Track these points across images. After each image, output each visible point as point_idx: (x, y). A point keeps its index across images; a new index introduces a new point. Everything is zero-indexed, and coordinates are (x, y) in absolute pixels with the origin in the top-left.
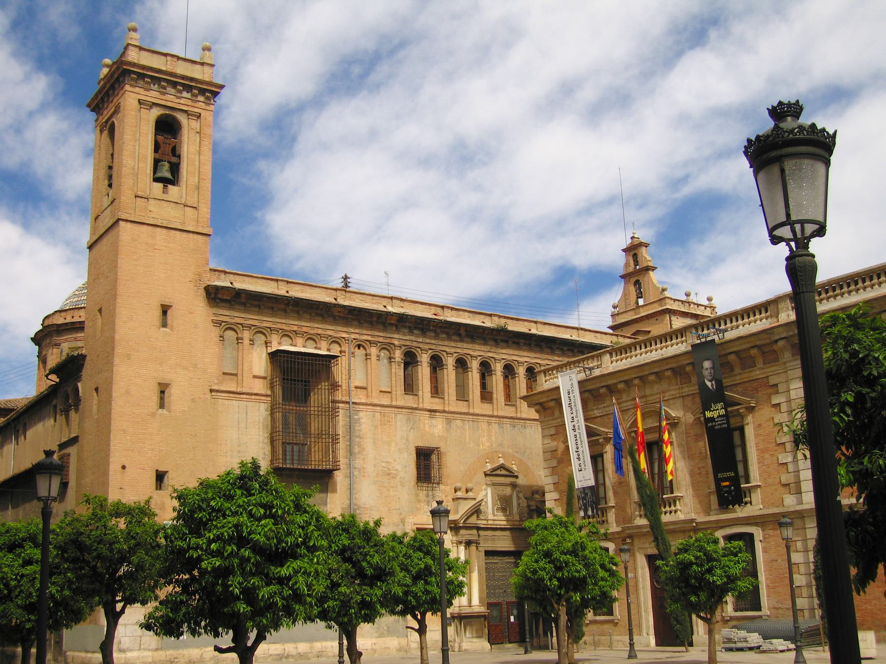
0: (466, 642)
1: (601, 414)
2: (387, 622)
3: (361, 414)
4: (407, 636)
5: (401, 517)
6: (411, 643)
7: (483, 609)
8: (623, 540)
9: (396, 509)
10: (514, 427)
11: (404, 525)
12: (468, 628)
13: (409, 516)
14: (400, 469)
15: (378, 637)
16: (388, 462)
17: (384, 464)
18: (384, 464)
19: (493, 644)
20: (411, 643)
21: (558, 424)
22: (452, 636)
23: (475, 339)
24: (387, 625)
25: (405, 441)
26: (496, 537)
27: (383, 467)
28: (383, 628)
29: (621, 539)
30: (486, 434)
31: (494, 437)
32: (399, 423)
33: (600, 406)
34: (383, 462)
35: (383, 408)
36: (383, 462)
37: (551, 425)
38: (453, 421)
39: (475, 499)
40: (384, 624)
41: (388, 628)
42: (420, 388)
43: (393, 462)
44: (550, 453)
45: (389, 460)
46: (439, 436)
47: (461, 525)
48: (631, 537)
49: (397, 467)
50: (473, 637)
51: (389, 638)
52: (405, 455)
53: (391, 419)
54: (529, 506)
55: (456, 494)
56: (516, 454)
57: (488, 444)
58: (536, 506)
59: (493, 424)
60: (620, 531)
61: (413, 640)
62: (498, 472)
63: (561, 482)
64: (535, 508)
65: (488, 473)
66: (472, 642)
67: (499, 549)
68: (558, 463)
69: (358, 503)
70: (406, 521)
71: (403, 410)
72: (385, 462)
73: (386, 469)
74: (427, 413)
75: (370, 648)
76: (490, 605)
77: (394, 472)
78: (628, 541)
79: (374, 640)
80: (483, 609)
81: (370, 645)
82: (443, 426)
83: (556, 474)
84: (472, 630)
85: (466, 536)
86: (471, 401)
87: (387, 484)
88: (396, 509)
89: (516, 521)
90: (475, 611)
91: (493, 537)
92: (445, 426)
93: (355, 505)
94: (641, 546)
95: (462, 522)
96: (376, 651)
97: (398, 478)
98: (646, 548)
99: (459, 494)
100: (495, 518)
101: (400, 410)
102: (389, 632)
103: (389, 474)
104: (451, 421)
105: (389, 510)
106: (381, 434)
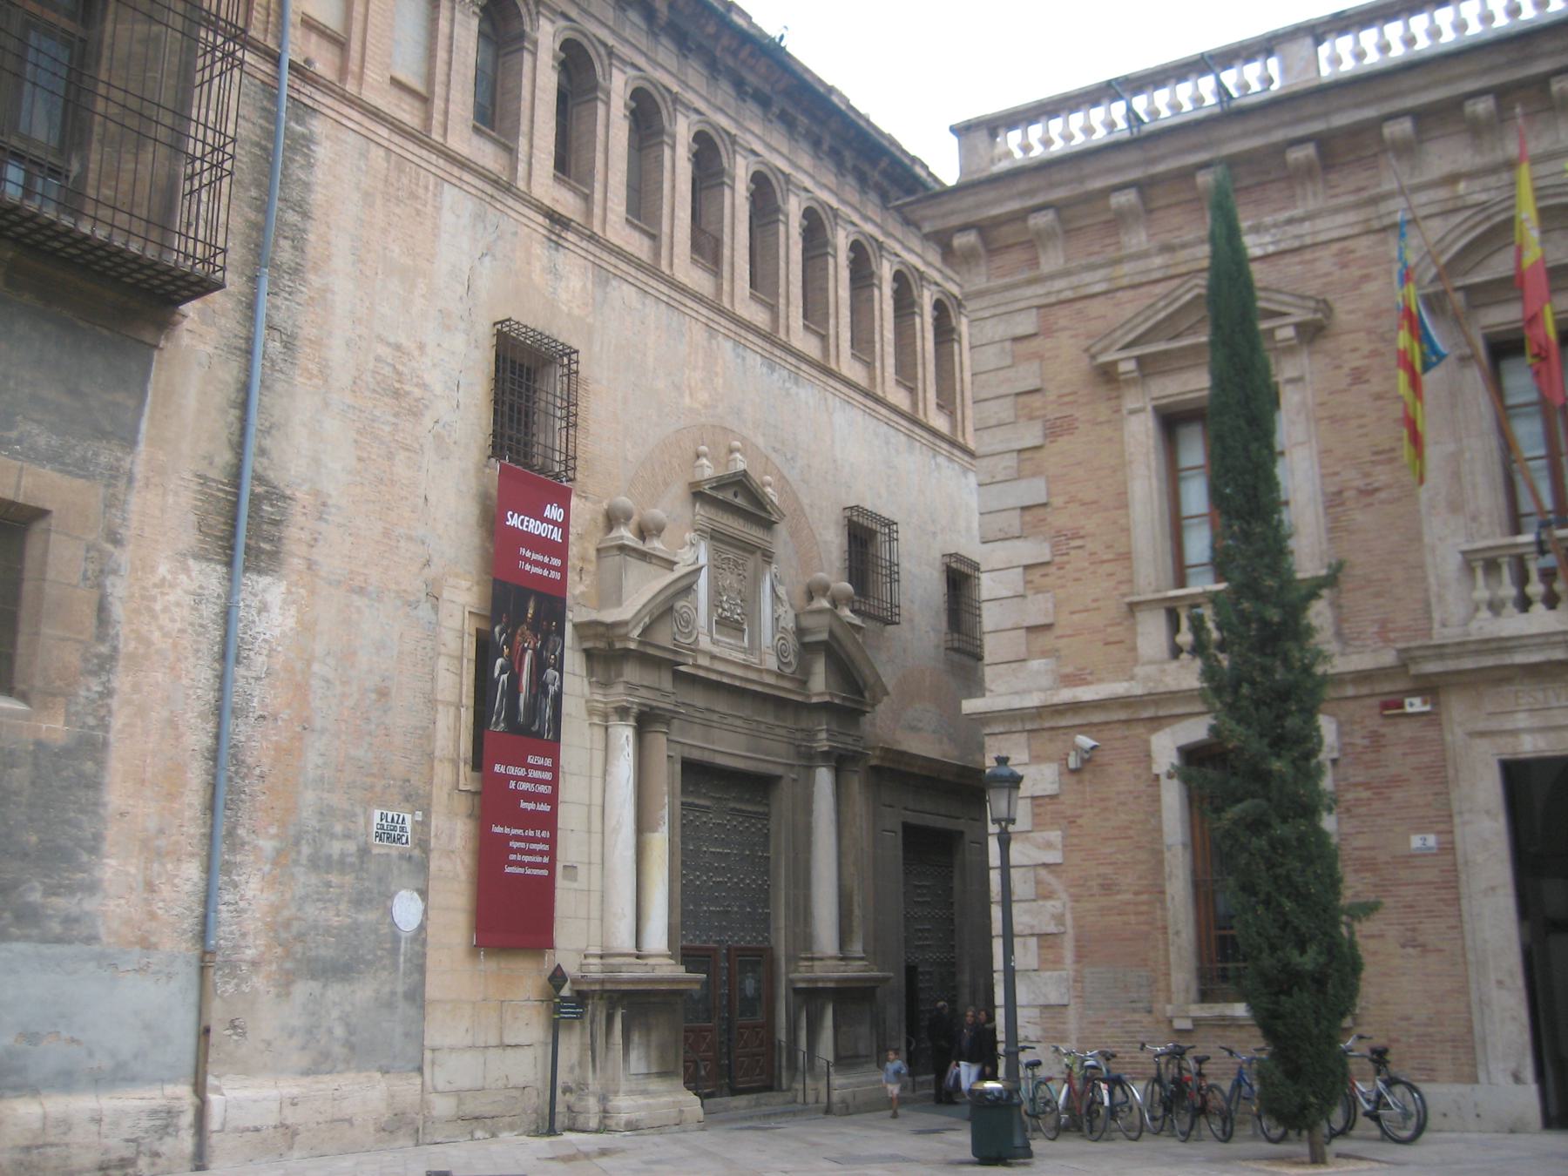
0: (631, 1093)
1: (1271, 249)
2: (348, 1008)
3: (318, 126)
4: (420, 1070)
5: (429, 573)
6: (434, 1097)
7: (668, 969)
8: (1386, 706)
9: (410, 538)
10: (773, 370)
11: (435, 609)
12: (636, 1038)
13: (457, 576)
14: (438, 388)
15: (306, 1073)
16: (398, 347)
17: (383, 350)
18: (383, 350)
19: (709, 1096)
20: (434, 1097)
21: (1053, 299)
22: (572, 1069)
23: (690, 50)
24: (345, 1019)
25: (462, 290)
26: (715, 717)
27: (378, 359)
28: (330, 1031)
29: (1376, 701)
30: (701, 364)
31: (721, 381)
32: (447, 217)
33: (1268, 220)
34: (380, 339)
35: (397, 139)
36: (380, 339)
37: (1022, 304)
38: (615, 283)
39: (670, 564)
40: (335, 1013)
41: (351, 1030)
42: (524, 127)
43: (416, 353)
44: (1009, 401)
45: (403, 340)
46: (569, 315)
47: (632, 646)
48: (1430, 688)
49: (428, 378)
50: (648, 1075)
51: (351, 1075)
52: (458, 342)
53: (421, 191)
54: (800, 631)
55: (614, 534)
56: (773, 456)
57: (704, 396)
58: (831, 633)
59: (720, 338)
60: (1391, 668)
61: (441, 1086)
62: (728, 496)
63: (1058, 501)
64: (824, 636)
65: (706, 488)
66: (644, 1093)
67: (721, 760)
68: (1045, 436)
69: (271, 475)
70: (446, 594)
71: (467, 177)
72: (389, 344)
73: (387, 371)
74: (540, 219)
75: (272, 1120)
76: (688, 956)
77: (417, 392)
78: (1415, 705)
79: (291, 1087)
80: (668, 969)
81: (275, 1106)
82: (584, 287)
83: (1034, 475)
84: (648, 1046)
85: (643, 692)
86: (665, 240)
87: (387, 429)
88: (410, 538)
89: (769, 671)
90: (659, 973)
91: (708, 715)
92: (589, 286)
93: (259, 479)
94: (1481, 725)
95: (635, 633)
96: (295, 1134)
97: (428, 421)
98: (1514, 733)
99: (626, 534)
100: (716, 650)
101: (456, 171)
102: (352, 1048)
103: (397, 394)
104: (607, 281)
105: (386, 534)
106: (384, 231)
